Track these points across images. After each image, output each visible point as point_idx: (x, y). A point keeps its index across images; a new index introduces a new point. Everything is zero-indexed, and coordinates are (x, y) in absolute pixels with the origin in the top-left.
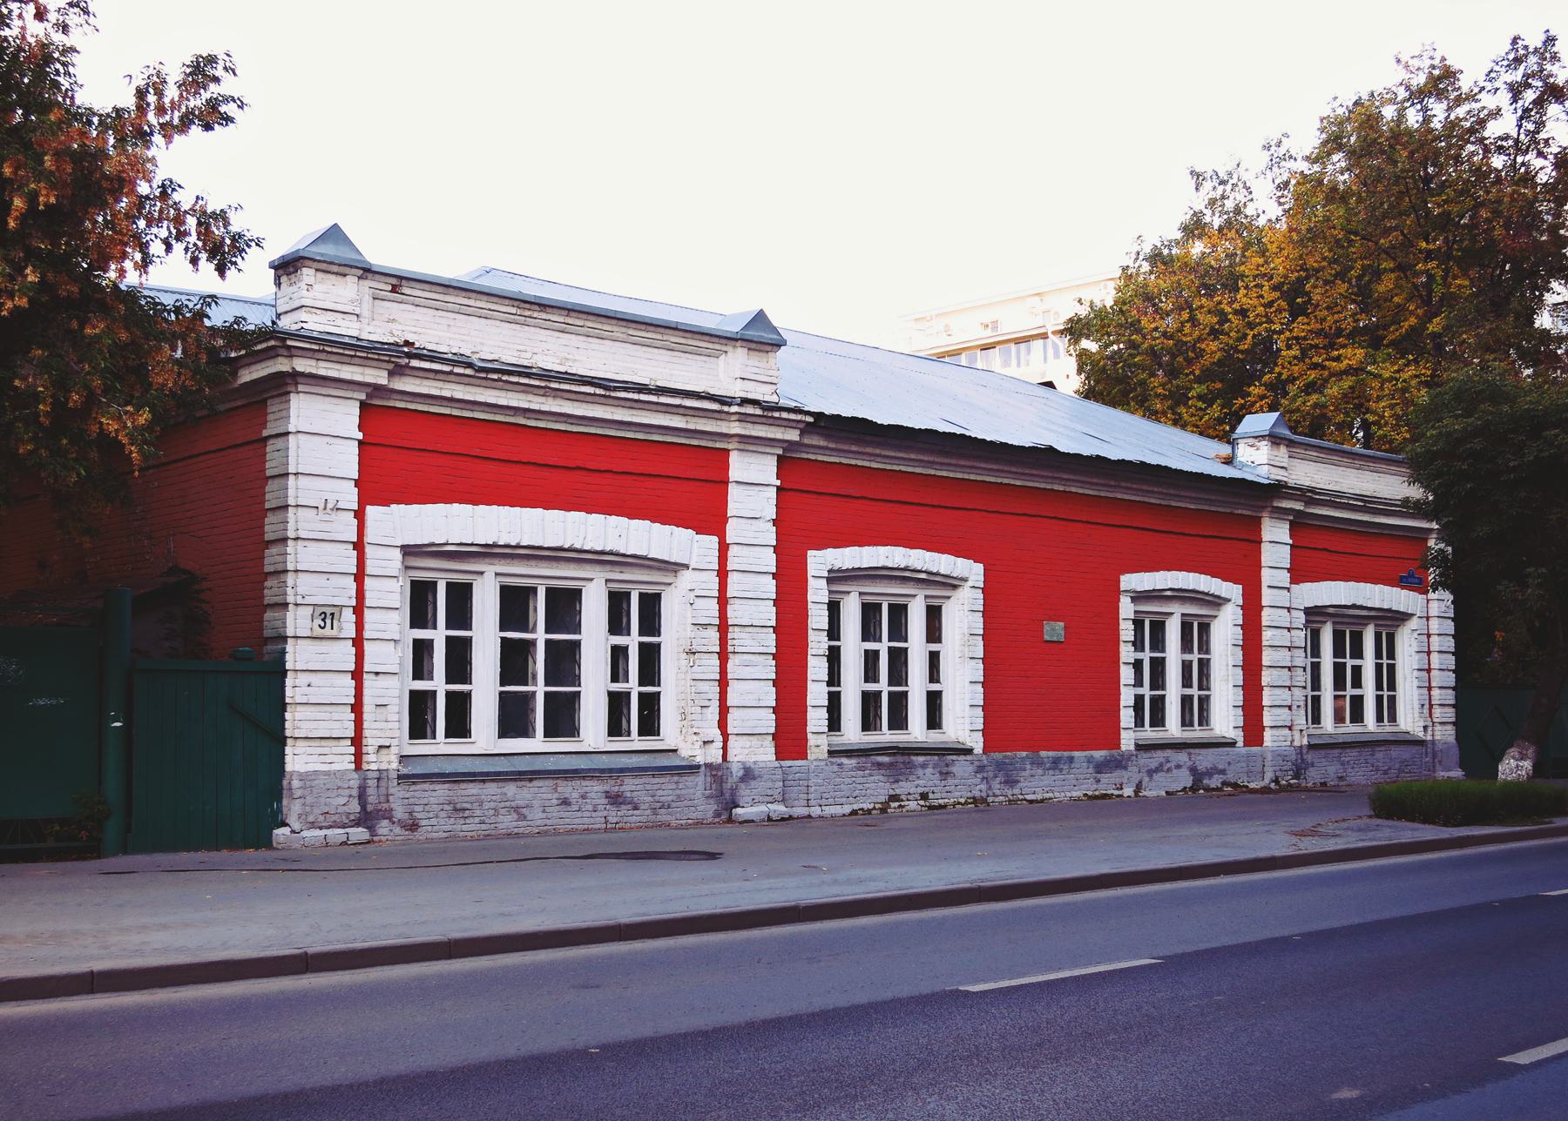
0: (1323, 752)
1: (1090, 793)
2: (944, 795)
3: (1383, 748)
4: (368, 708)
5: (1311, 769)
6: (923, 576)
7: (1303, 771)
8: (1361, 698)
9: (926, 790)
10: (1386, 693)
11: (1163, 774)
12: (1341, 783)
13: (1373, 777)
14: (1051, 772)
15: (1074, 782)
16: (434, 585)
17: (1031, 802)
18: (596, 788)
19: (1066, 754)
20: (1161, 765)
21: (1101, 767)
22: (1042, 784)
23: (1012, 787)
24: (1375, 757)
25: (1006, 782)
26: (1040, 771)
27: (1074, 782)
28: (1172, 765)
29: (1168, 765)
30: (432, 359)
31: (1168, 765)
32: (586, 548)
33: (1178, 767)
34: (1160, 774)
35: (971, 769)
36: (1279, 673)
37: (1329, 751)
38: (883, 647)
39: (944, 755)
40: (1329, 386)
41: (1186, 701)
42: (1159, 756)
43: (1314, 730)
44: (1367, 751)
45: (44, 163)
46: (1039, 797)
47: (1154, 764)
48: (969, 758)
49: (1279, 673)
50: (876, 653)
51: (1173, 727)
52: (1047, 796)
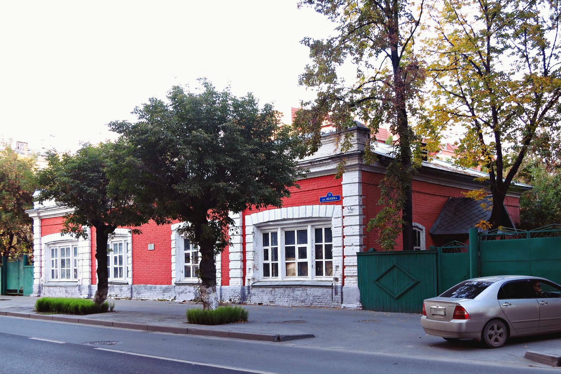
0: (261, 289)
1: (160, 299)
2: (121, 296)
3: (301, 289)
4: (42, 273)
5: (253, 296)
6: (119, 235)
7: (249, 297)
8: (69, 270)
9: (117, 294)
10: (270, 261)
11: (184, 294)
12: (272, 304)
13: (294, 303)
14: (150, 291)
15: (156, 295)
16: (321, 229)
17: (142, 300)
18: (64, 289)
19: (154, 286)
20: (183, 291)
21: (165, 291)
22: (147, 295)
23: (139, 295)
24: (295, 293)
25: (138, 293)
26: (146, 291)
27: (156, 295)
28: (187, 291)
29: (186, 291)
30: (49, 208)
31: (186, 291)
32: (307, 216)
33: (190, 292)
34: (182, 294)
35: (127, 289)
36: (234, 255)
37: (264, 289)
38: (269, 248)
39: (291, 287)
40: (97, 163)
41: (116, 269)
42: (183, 287)
43: (326, 278)
44: (288, 291)
45: (320, 128)
46: (145, 299)
47: (181, 291)
48: (127, 286)
49: (234, 255)
50: (267, 250)
51: (72, 278)
52: (148, 298)
